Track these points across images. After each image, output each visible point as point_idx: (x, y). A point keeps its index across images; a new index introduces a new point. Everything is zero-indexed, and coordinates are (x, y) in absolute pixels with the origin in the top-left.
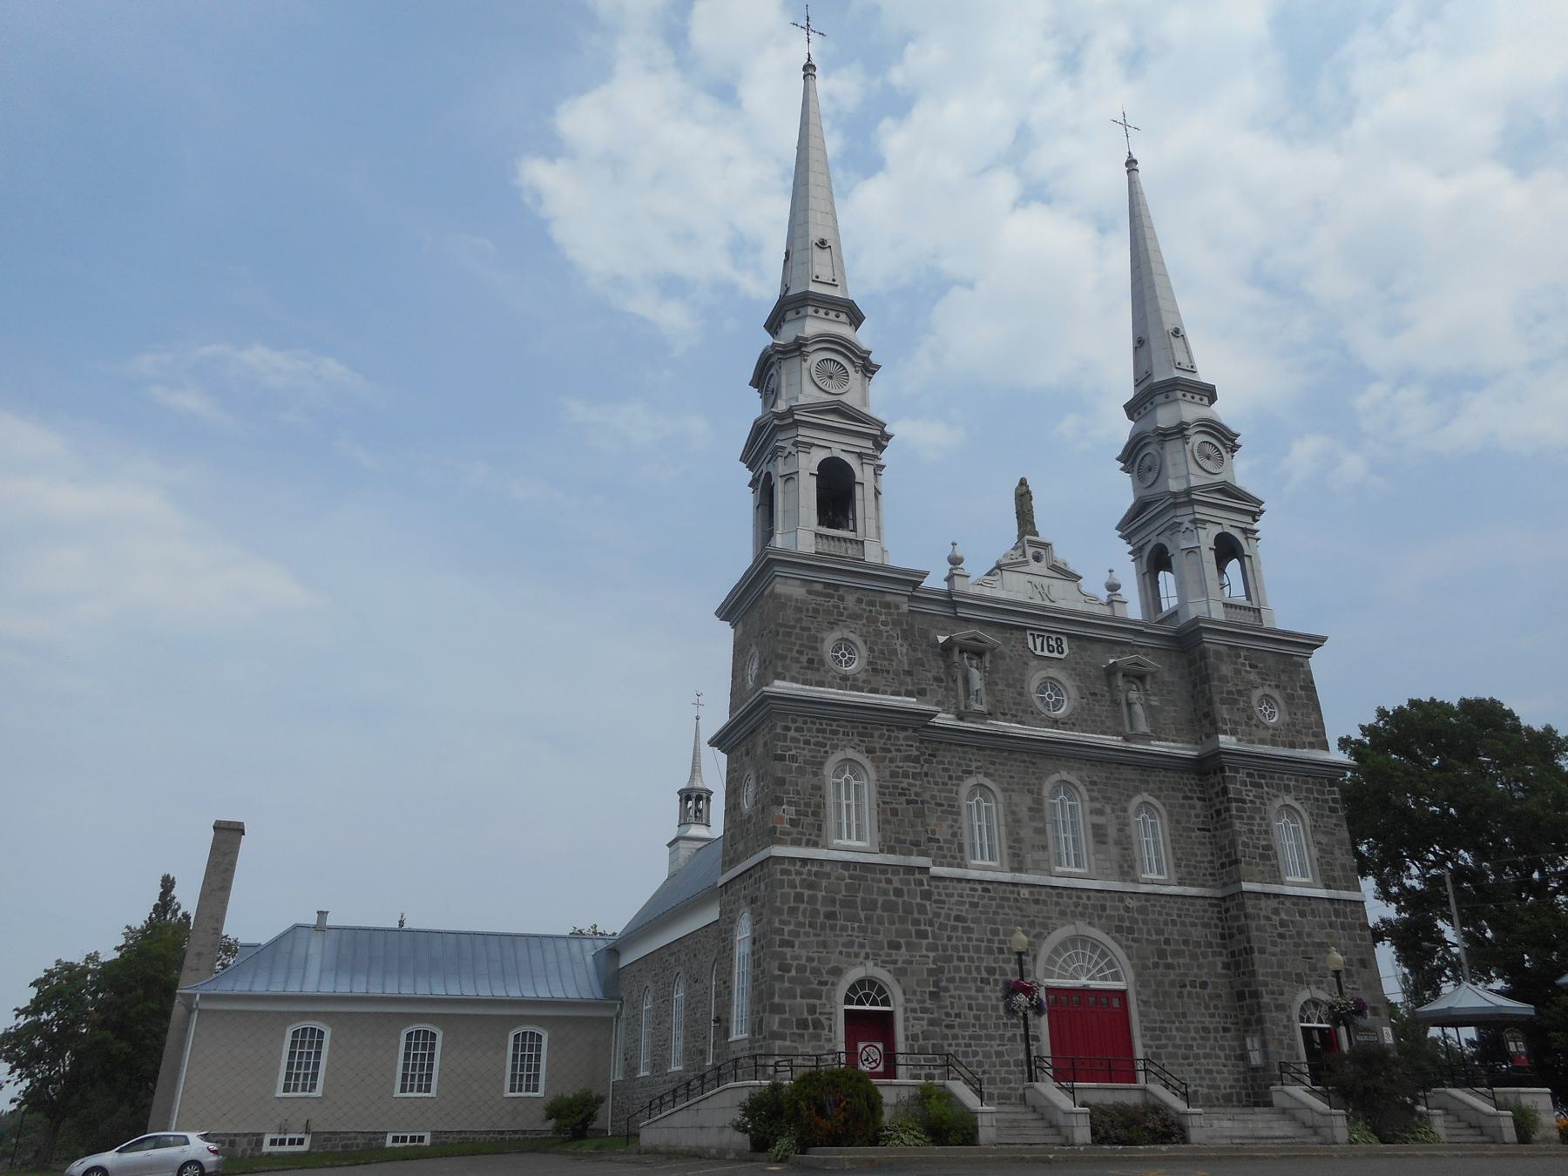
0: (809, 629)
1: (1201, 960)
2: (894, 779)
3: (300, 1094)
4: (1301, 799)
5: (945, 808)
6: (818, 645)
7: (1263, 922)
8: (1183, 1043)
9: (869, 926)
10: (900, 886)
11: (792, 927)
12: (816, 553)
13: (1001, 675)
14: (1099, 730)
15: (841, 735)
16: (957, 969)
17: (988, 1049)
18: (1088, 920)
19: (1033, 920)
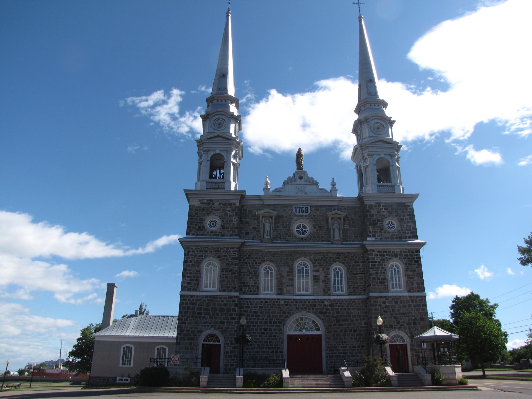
0: (200, 216)
1: (355, 322)
2: (228, 266)
3: (126, 366)
5: (253, 274)
7: (378, 307)
10: (226, 303)
11: (186, 318)
13: (281, 224)
15: (209, 252)
17: (262, 356)
18: (307, 310)
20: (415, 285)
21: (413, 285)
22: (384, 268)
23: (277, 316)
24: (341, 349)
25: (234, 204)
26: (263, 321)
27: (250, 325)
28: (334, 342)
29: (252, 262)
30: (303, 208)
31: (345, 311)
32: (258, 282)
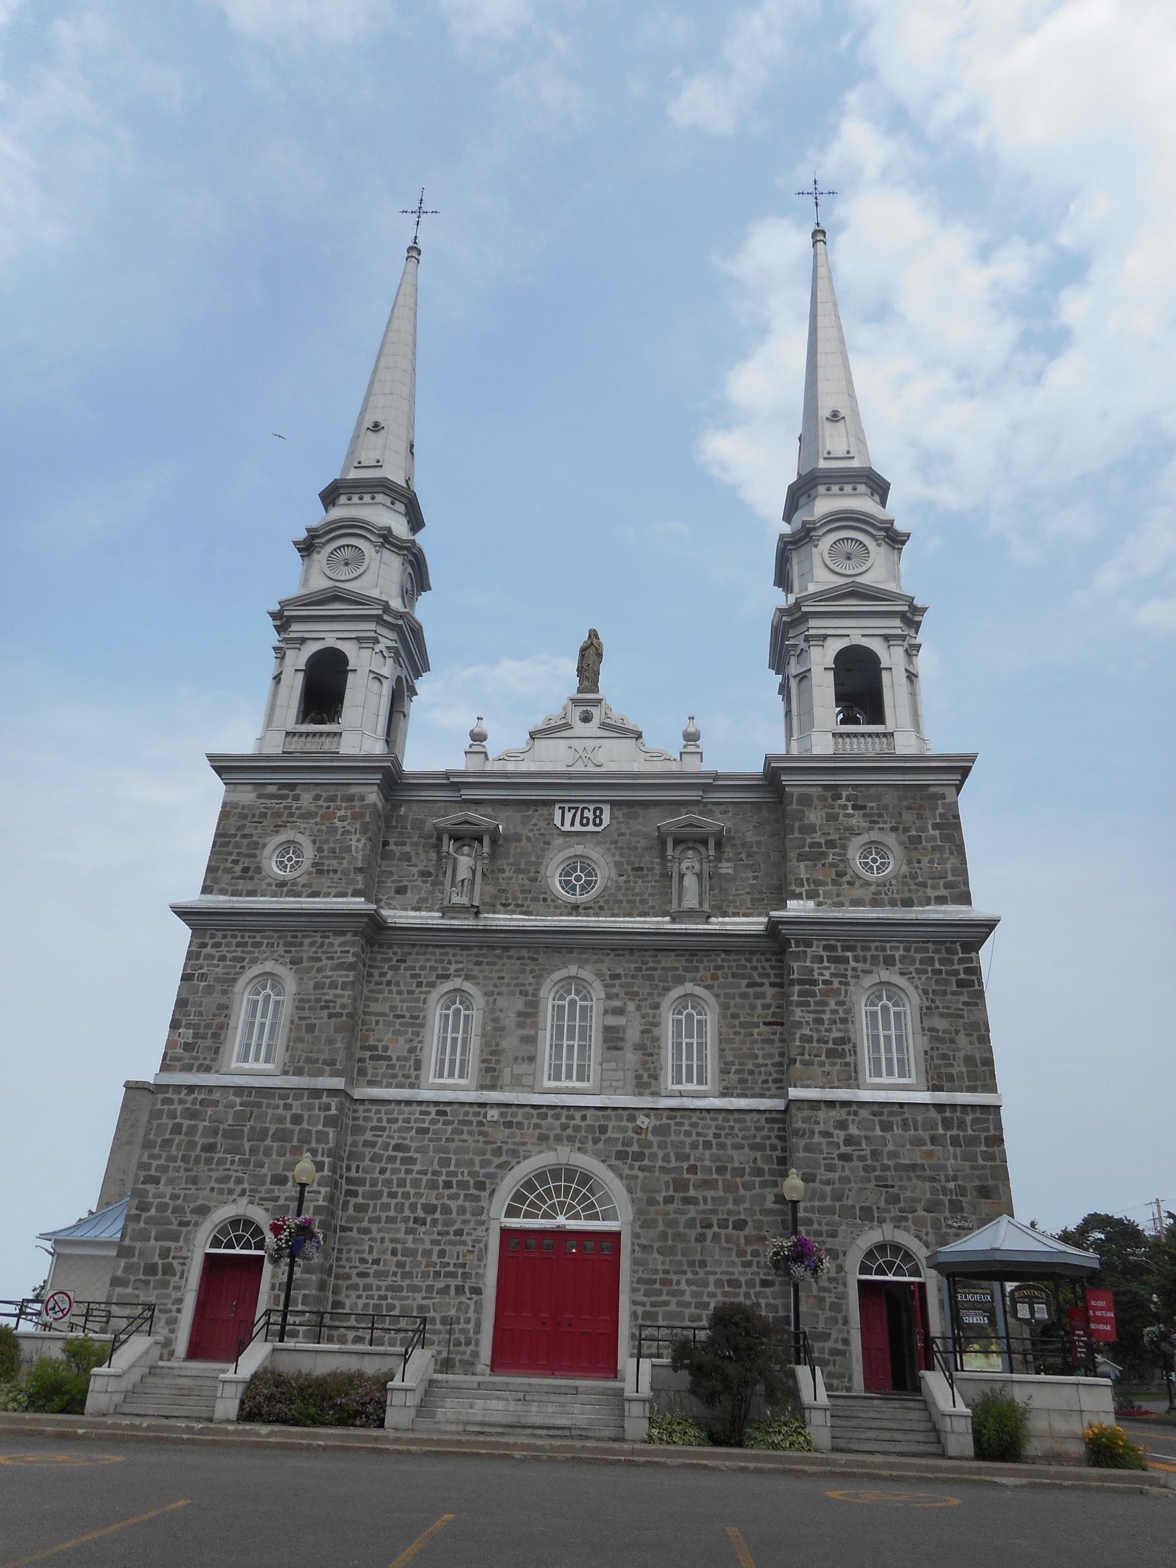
1: (742, 1192)
4: (911, 973)
6: (257, 852)
8: (693, 1300)
9: (253, 1159)
10: (299, 1112)
11: (162, 1162)
12: (284, 753)
13: (511, 860)
14: (636, 912)
15: (263, 948)
16: (385, 1207)
17: (408, 1302)
18: (577, 1145)
19: (500, 1147)
20: (959, 1068)
21: (952, 1065)
22: (843, 1003)
23: (472, 1162)
24: (688, 1290)
25: (362, 798)
26: (425, 1178)
27: (381, 1192)
29: (408, 979)
30: (586, 811)
31: (707, 1152)
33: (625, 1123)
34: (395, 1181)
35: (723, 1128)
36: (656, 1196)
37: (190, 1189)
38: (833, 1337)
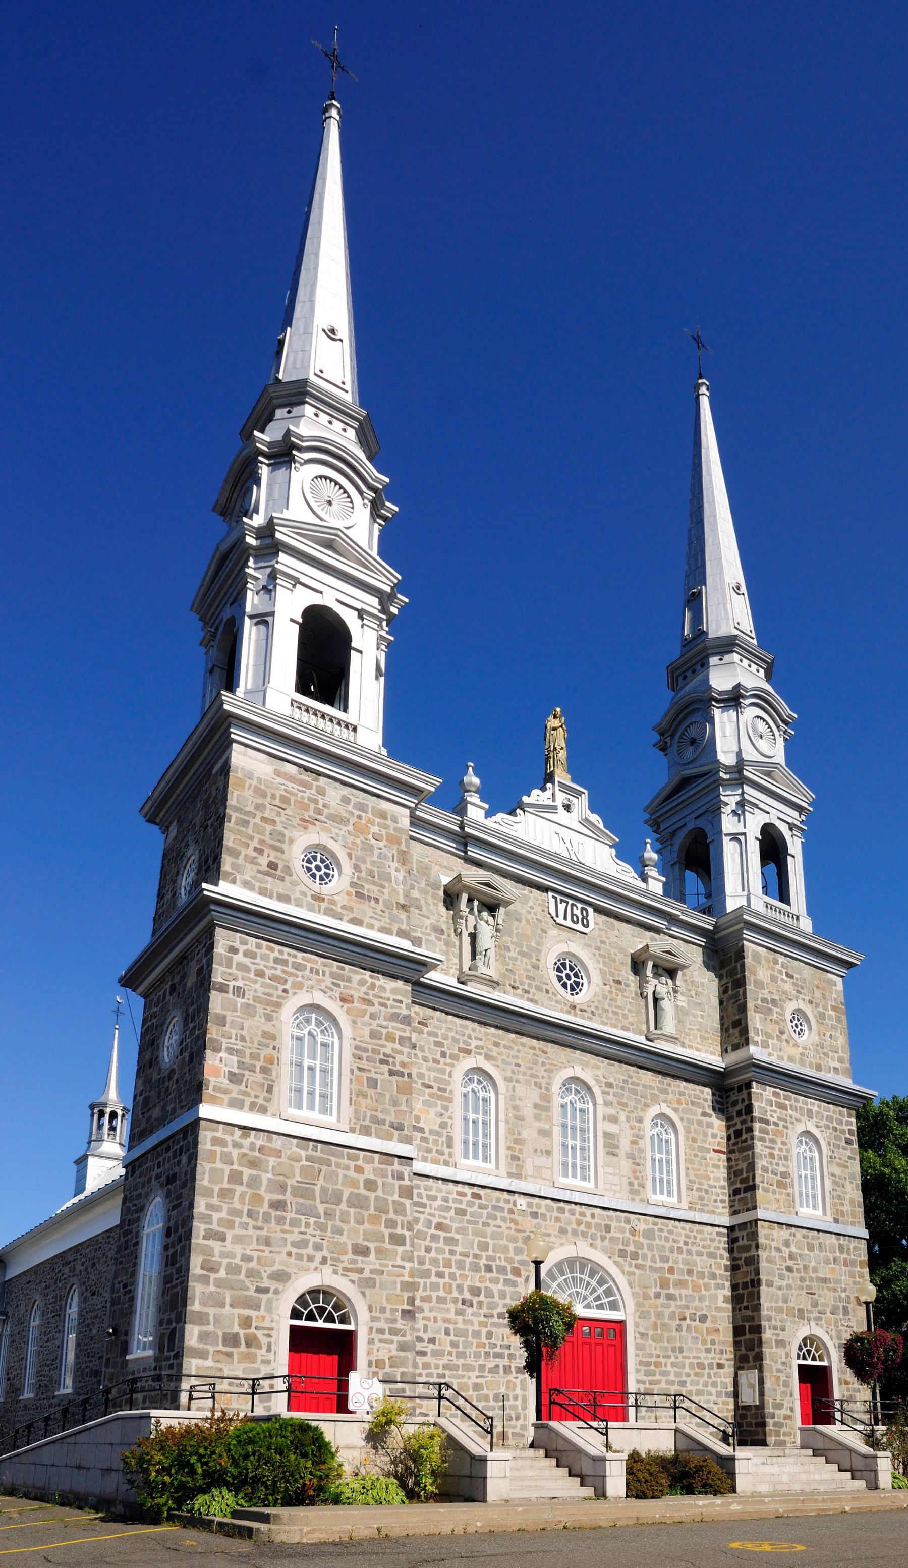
9: (330, 1224)
10: (372, 1177)
11: (224, 1215)
13: (515, 939)
16: (435, 1287)
17: (464, 1380)
18: (589, 1241)
23: (506, 1249)
28: (655, 1349)
32: (450, 1122)
33: (623, 1225)
34: (441, 1261)
35: (689, 1237)
36: (648, 1291)
37: (263, 1251)
38: (785, 1406)
